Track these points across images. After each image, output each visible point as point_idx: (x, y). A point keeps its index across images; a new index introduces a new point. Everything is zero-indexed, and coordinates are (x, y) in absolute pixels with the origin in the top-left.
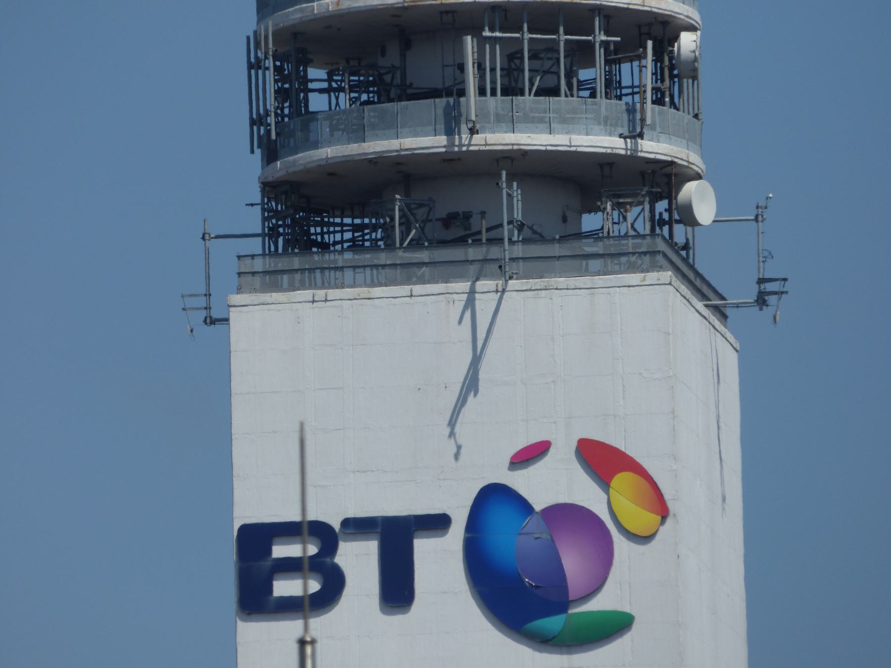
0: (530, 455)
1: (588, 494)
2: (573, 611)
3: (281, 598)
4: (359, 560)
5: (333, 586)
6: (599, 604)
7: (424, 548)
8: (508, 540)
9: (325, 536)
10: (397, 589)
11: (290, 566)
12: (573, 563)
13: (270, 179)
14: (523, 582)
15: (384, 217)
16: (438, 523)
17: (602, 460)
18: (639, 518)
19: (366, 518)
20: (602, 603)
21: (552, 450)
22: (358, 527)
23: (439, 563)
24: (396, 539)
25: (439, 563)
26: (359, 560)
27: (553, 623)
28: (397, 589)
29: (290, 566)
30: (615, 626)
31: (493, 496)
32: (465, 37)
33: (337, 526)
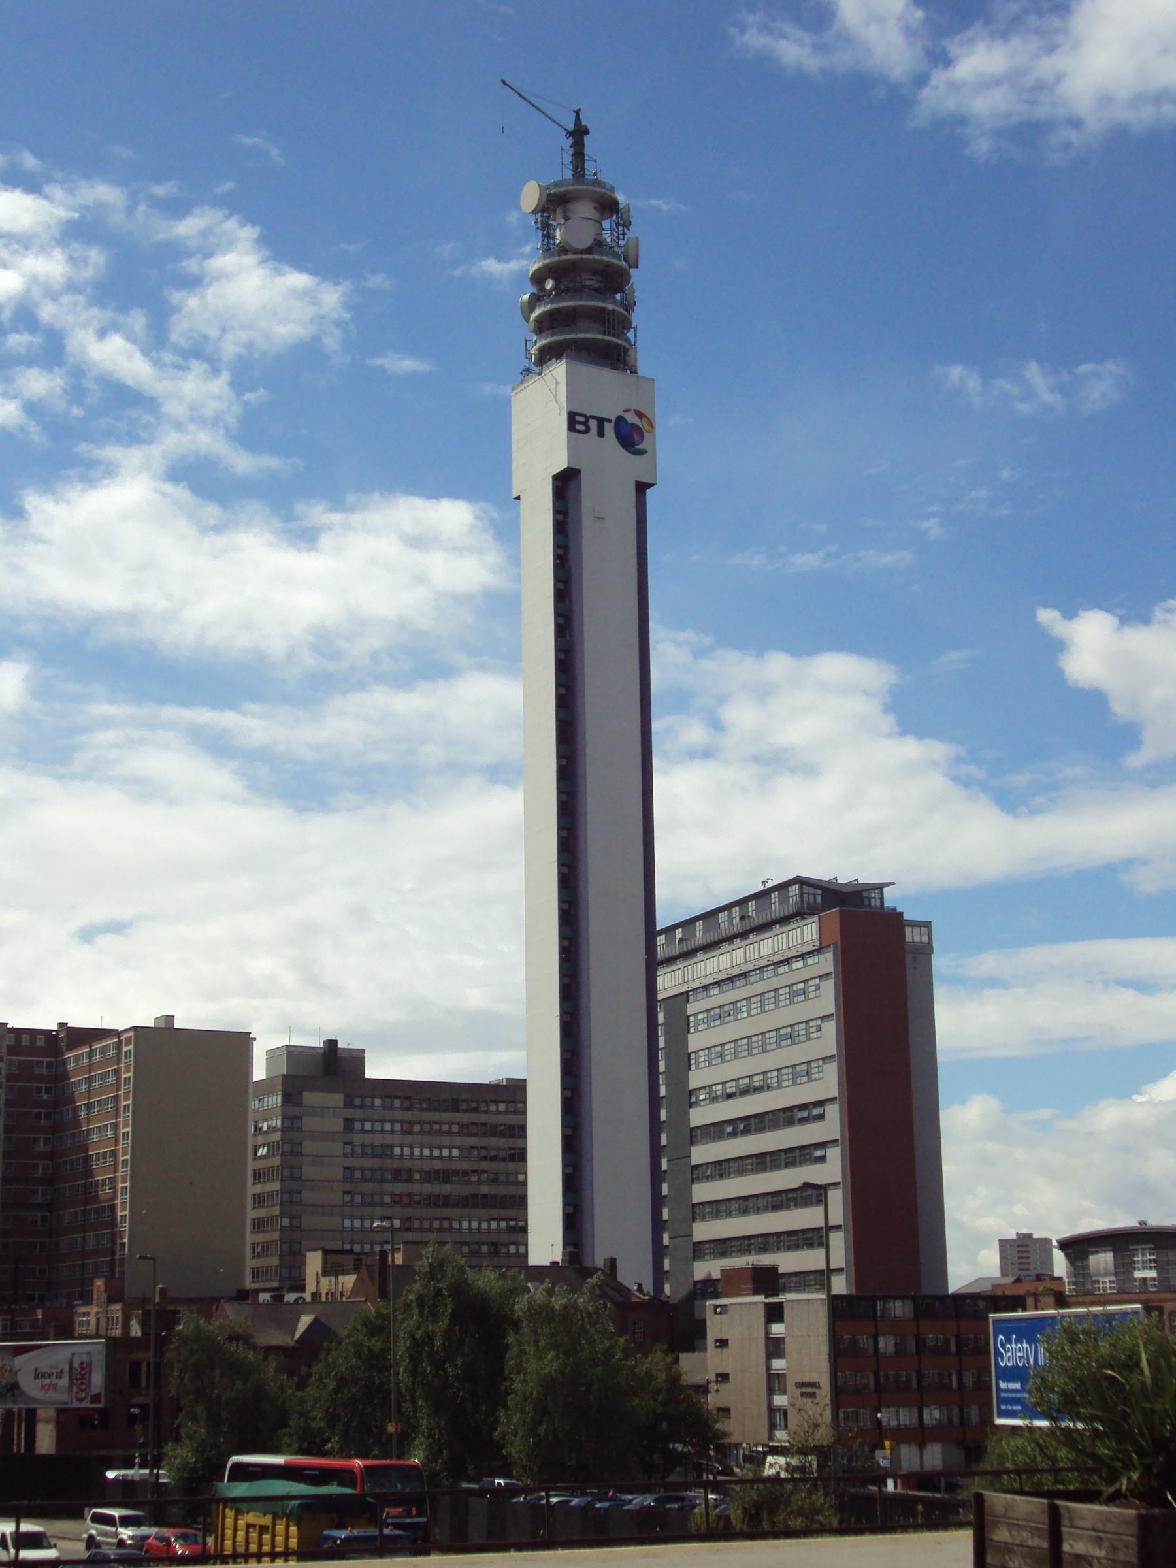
0: (626, 411)
1: (637, 421)
4: (593, 424)
5: (587, 430)
6: (640, 447)
7: (606, 424)
9: (587, 418)
10: (601, 434)
11: (580, 423)
13: (323, 1320)
14: (37, 154)
16: (609, 421)
17: (640, 415)
18: (647, 427)
20: (640, 447)
23: (609, 429)
24: (601, 422)
25: (609, 429)
26: (593, 424)
28: (601, 434)
29: (580, 423)
30: (642, 453)
31: (620, 419)
33: (225, 377)
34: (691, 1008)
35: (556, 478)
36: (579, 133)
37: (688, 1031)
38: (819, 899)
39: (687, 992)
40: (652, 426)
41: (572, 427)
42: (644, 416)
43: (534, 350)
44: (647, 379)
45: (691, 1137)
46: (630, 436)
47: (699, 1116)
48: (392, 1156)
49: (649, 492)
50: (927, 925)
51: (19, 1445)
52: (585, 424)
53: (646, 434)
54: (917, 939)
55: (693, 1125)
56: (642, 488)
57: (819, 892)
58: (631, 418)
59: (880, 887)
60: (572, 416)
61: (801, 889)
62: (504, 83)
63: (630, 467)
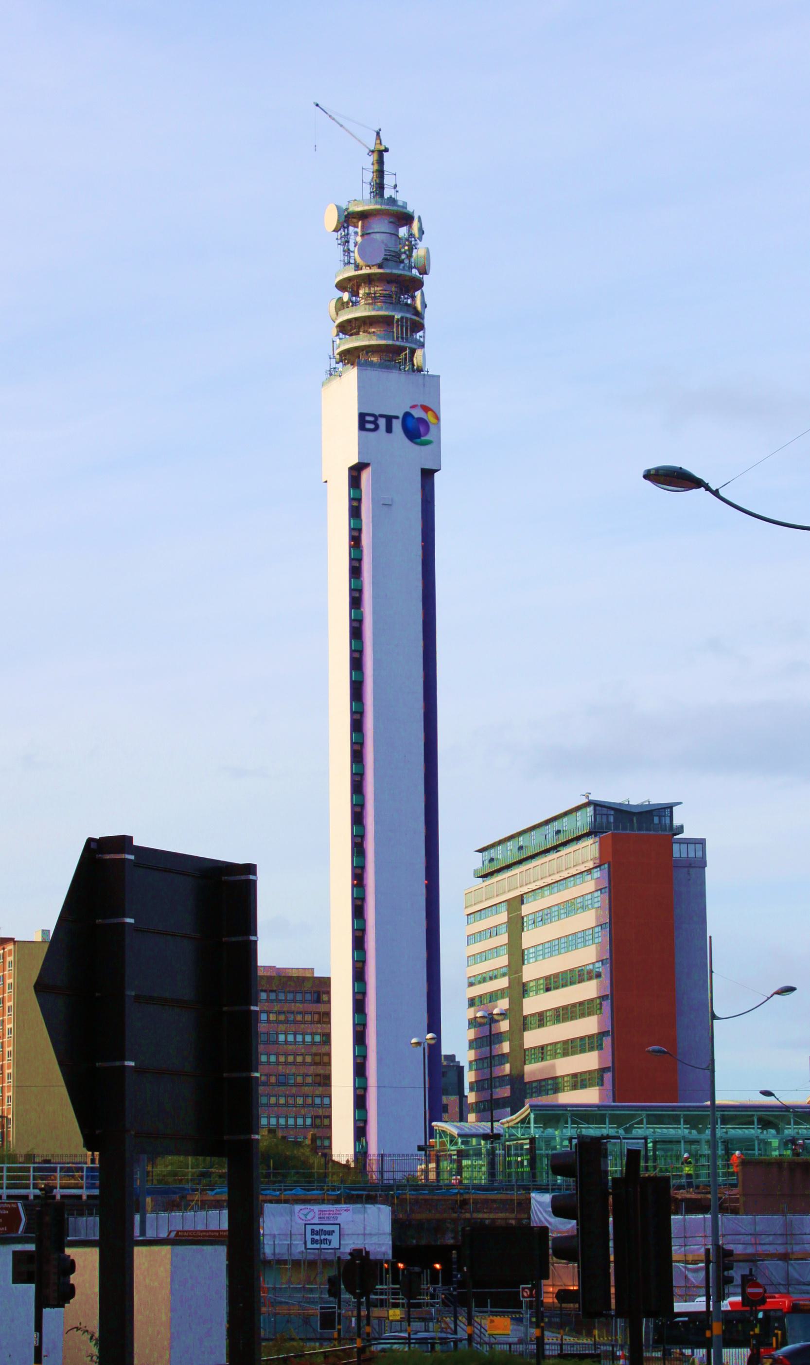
0: (413, 407)
2: (423, 438)
3: (261, 1213)
5: (377, 428)
7: (394, 421)
8: (410, 423)
10: (389, 429)
12: (422, 430)
15: (304, 1034)
16: (397, 417)
17: (426, 409)
19: (702, 895)
21: (653, 465)
22: (382, 416)
23: (397, 425)
24: (389, 419)
25: (397, 425)
26: (382, 422)
27: (418, 440)
28: (389, 429)
30: (428, 443)
31: (407, 415)
32: (225, 1160)
34: (526, 909)
35: (352, 469)
36: (380, 154)
37: (523, 930)
38: (612, 819)
39: (522, 895)
40: (438, 418)
41: (362, 426)
42: (431, 410)
43: (337, 351)
44: (433, 376)
45: (524, 1024)
46: (418, 428)
47: (532, 1005)
48: (277, 1042)
49: (436, 474)
50: (702, 842)
51: (227, 1233)
52: (375, 422)
53: (432, 428)
54: (692, 855)
55: (525, 1014)
56: (428, 475)
57: (612, 812)
58: (418, 413)
59: (670, 807)
60: (362, 417)
61: (595, 810)
62: (317, 105)
63: (413, 456)
